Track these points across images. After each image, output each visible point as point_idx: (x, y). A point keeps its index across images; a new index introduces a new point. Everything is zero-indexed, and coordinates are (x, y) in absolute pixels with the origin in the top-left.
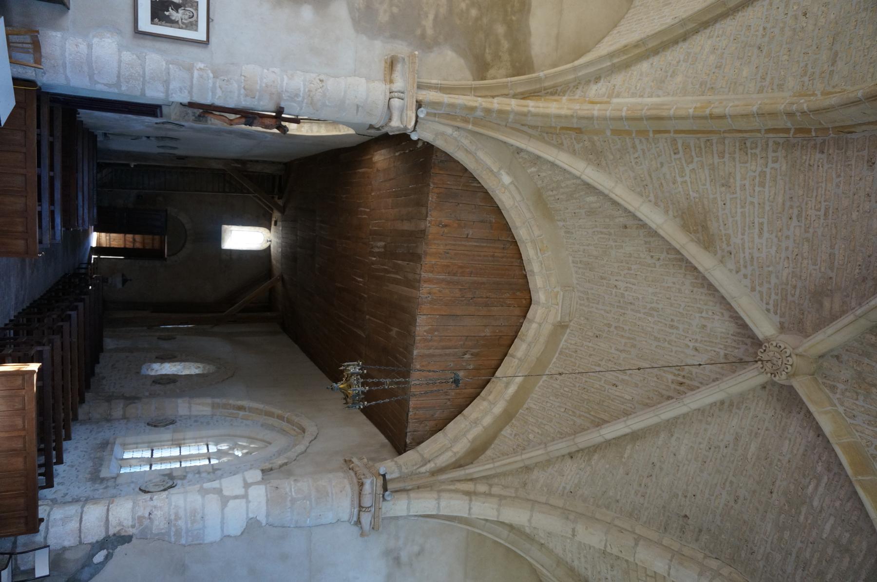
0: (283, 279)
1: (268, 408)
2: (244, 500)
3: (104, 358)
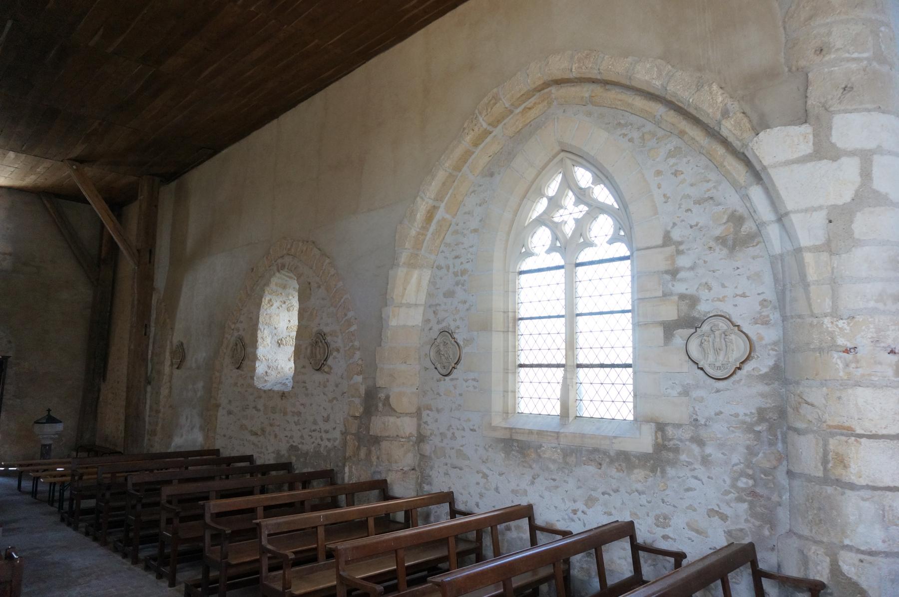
0: (80, 160)
1: (458, 152)
2: (876, 158)
3: (232, 443)
